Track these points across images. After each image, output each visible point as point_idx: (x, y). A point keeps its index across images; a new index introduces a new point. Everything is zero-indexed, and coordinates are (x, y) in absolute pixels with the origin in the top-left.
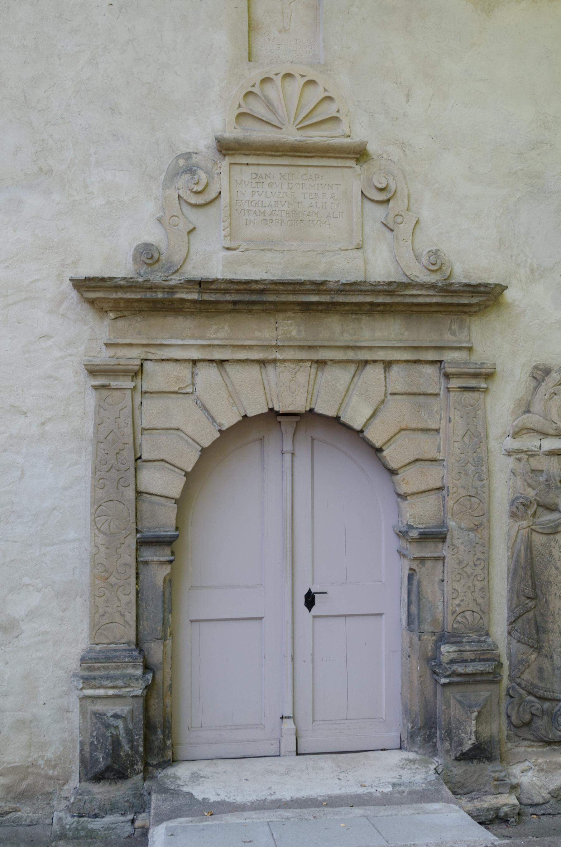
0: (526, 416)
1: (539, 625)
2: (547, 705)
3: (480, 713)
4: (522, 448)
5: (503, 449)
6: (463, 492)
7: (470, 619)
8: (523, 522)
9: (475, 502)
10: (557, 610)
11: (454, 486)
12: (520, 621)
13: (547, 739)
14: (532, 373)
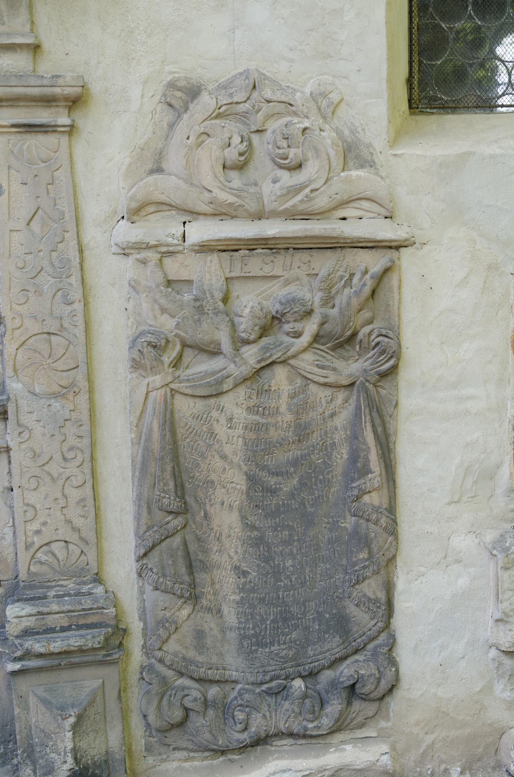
0: (151, 179)
1: (193, 558)
2: (213, 691)
3: (80, 718)
4: (147, 240)
5: (113, 244)
6: (34, 327)
7: (61, 555)
8: (154, 378)
9: (58, 345)
10: (227, 530)
11: (16, 316)
12: (156, 553)
13: (215, 747)
14: (164, 95)
